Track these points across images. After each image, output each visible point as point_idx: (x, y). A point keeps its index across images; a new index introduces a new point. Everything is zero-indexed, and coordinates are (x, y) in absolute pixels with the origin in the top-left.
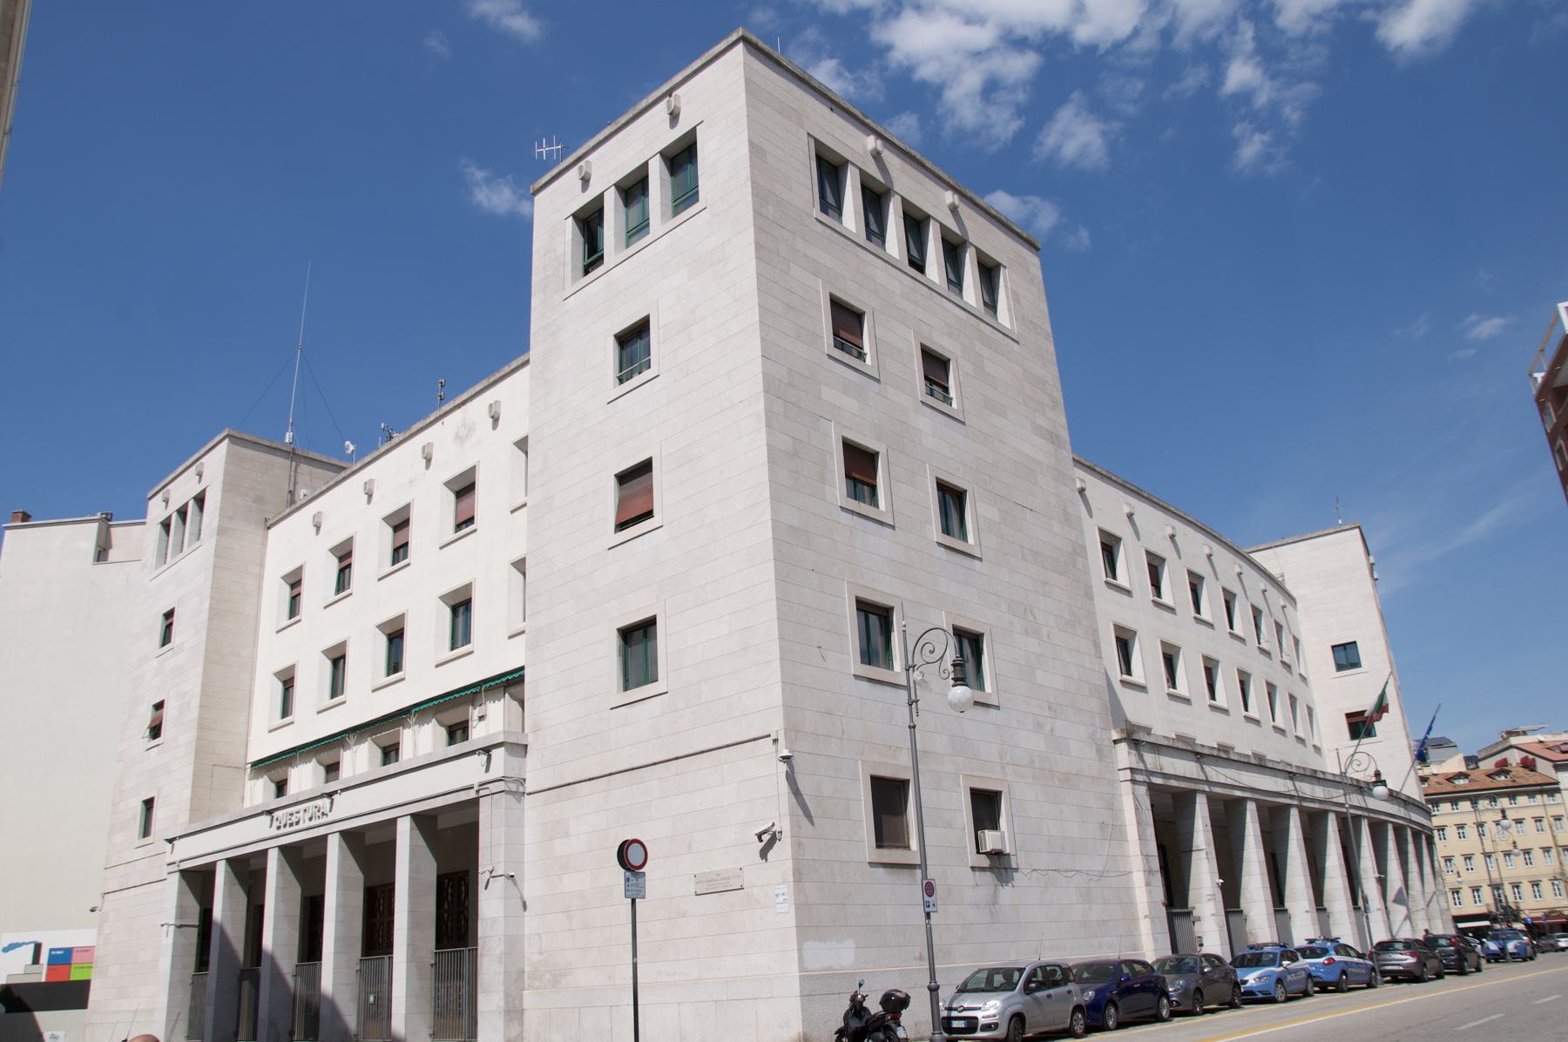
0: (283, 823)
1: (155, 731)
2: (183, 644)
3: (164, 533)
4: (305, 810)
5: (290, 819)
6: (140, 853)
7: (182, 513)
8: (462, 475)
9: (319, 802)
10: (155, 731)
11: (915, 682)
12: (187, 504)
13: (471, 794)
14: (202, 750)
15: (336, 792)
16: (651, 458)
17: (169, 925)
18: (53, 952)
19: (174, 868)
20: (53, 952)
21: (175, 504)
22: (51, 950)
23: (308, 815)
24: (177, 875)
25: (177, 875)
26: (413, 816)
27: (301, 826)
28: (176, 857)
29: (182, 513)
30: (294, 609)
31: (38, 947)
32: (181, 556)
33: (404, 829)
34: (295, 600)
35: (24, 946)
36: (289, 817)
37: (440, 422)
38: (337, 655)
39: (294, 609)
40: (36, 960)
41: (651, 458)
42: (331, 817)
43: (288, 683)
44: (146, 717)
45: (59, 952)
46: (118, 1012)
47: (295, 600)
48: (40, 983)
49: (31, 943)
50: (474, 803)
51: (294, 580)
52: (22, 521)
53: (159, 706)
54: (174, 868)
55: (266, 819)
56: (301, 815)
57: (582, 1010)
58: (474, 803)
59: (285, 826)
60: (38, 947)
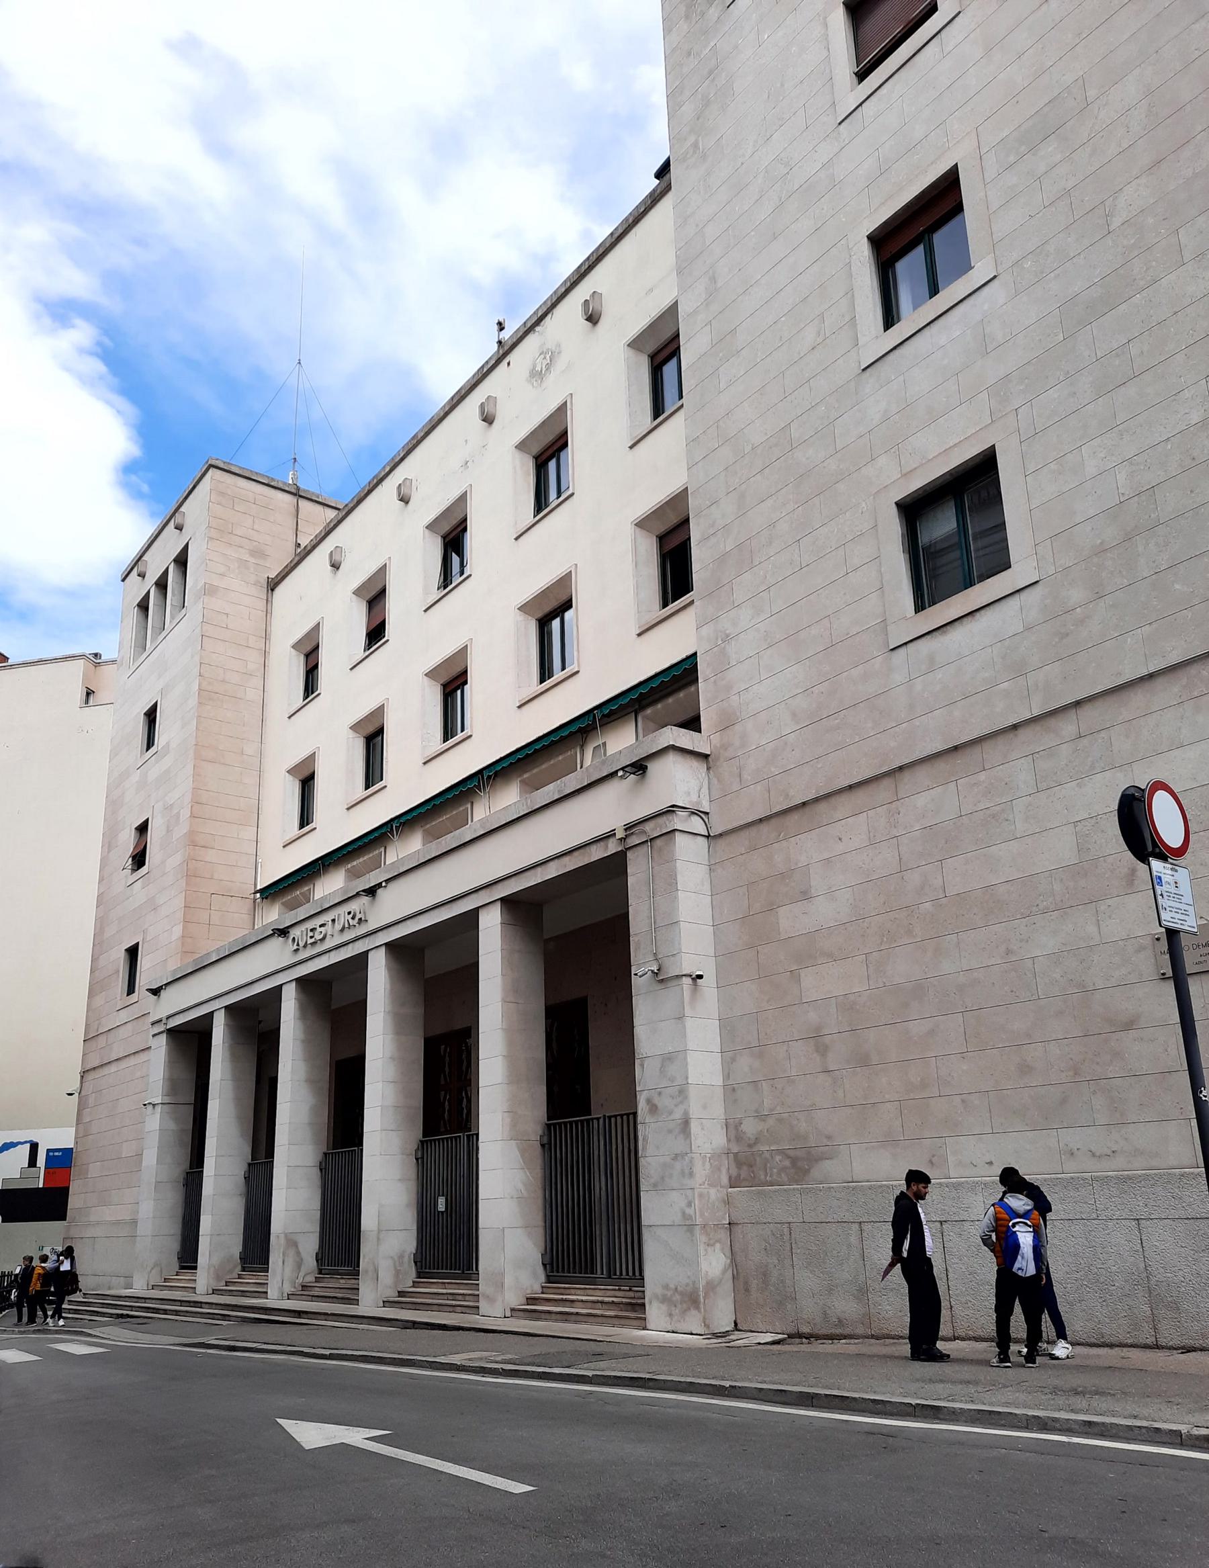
0: (302, 944)
1: (139, 859)
2: (168, 744)
3: (142, 617)
4: (333, 921)
5: (311, 937)
6: (124, 1016)
7: (162, 584)
8: (544, 424)
9: (354, 906)
10: (139, 859)
11: (214, 1292)
12: (166, 571)
13: (613, 847)
14: (191, 874)
15: (379, 885)
16: (956, 165)
17: (154, 1105)
18: (51, 1154)
19: (161, 1028)
20: (51, 1154)
21: (153, 576)
22: (48, 1151)
23: (338, 927)
24: (164, 1036)
25: (163, 1039)
26: (504, 901)
27: (329, 944)
28: (162, 1013)
29: (162, 584)
30: (310, 687)
31: (34, 1147)
32: (164, 634)
33: (491, 924)
34: (311, 673)
35: (20, 1146)
36: (311, 934)
37: (505, 362)
38: (371, 729)
39: (310, 687)
40: (32, 1162)
41: (956, 165)
42: (372, 925)
43: (307, 783)
44: (127, 842)
45: (56, 1154)
46: (98, 1223)
47: (311, 673)
48: (38, 1188)
49: (26, 1142)
50: (615, 867)
51: (309, 648)
52: (266, 1159)
53: (143, 829)
54: (157, 1029)
55: (277, 941)
56: (329, 929)
57: (865, 1227)
58: (615, 867)
59: (305, 946)
60: (34, 1147)
